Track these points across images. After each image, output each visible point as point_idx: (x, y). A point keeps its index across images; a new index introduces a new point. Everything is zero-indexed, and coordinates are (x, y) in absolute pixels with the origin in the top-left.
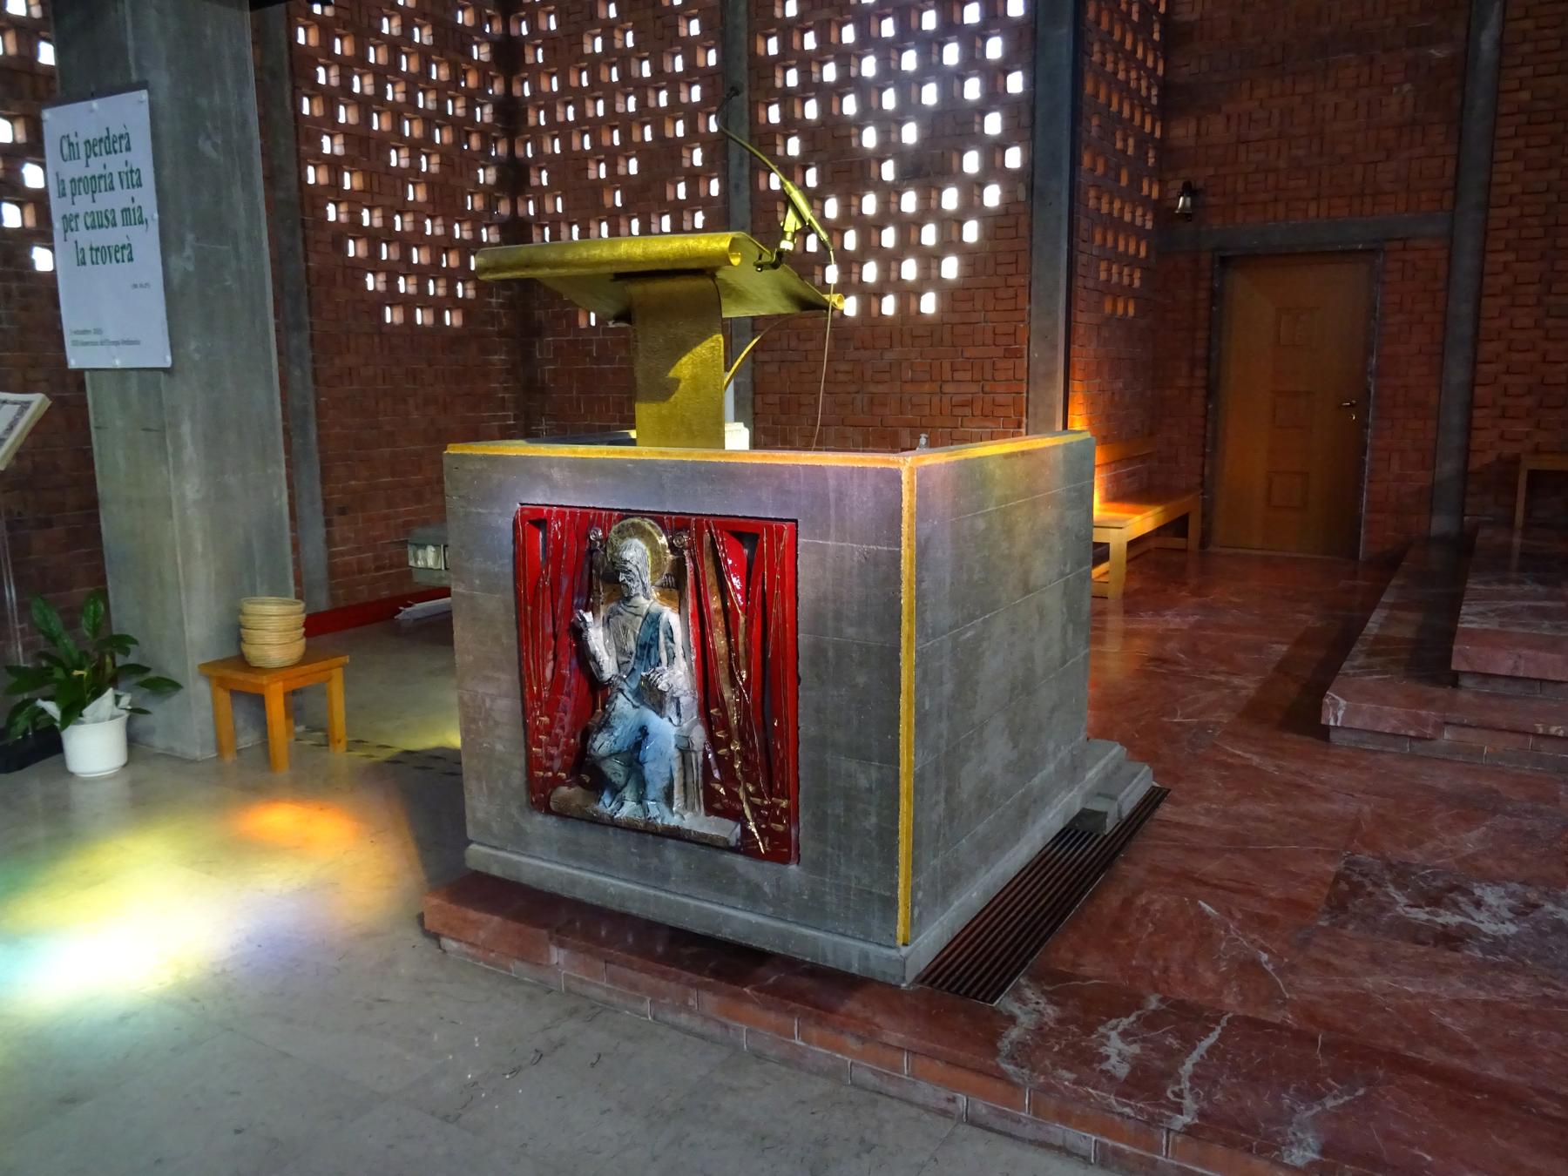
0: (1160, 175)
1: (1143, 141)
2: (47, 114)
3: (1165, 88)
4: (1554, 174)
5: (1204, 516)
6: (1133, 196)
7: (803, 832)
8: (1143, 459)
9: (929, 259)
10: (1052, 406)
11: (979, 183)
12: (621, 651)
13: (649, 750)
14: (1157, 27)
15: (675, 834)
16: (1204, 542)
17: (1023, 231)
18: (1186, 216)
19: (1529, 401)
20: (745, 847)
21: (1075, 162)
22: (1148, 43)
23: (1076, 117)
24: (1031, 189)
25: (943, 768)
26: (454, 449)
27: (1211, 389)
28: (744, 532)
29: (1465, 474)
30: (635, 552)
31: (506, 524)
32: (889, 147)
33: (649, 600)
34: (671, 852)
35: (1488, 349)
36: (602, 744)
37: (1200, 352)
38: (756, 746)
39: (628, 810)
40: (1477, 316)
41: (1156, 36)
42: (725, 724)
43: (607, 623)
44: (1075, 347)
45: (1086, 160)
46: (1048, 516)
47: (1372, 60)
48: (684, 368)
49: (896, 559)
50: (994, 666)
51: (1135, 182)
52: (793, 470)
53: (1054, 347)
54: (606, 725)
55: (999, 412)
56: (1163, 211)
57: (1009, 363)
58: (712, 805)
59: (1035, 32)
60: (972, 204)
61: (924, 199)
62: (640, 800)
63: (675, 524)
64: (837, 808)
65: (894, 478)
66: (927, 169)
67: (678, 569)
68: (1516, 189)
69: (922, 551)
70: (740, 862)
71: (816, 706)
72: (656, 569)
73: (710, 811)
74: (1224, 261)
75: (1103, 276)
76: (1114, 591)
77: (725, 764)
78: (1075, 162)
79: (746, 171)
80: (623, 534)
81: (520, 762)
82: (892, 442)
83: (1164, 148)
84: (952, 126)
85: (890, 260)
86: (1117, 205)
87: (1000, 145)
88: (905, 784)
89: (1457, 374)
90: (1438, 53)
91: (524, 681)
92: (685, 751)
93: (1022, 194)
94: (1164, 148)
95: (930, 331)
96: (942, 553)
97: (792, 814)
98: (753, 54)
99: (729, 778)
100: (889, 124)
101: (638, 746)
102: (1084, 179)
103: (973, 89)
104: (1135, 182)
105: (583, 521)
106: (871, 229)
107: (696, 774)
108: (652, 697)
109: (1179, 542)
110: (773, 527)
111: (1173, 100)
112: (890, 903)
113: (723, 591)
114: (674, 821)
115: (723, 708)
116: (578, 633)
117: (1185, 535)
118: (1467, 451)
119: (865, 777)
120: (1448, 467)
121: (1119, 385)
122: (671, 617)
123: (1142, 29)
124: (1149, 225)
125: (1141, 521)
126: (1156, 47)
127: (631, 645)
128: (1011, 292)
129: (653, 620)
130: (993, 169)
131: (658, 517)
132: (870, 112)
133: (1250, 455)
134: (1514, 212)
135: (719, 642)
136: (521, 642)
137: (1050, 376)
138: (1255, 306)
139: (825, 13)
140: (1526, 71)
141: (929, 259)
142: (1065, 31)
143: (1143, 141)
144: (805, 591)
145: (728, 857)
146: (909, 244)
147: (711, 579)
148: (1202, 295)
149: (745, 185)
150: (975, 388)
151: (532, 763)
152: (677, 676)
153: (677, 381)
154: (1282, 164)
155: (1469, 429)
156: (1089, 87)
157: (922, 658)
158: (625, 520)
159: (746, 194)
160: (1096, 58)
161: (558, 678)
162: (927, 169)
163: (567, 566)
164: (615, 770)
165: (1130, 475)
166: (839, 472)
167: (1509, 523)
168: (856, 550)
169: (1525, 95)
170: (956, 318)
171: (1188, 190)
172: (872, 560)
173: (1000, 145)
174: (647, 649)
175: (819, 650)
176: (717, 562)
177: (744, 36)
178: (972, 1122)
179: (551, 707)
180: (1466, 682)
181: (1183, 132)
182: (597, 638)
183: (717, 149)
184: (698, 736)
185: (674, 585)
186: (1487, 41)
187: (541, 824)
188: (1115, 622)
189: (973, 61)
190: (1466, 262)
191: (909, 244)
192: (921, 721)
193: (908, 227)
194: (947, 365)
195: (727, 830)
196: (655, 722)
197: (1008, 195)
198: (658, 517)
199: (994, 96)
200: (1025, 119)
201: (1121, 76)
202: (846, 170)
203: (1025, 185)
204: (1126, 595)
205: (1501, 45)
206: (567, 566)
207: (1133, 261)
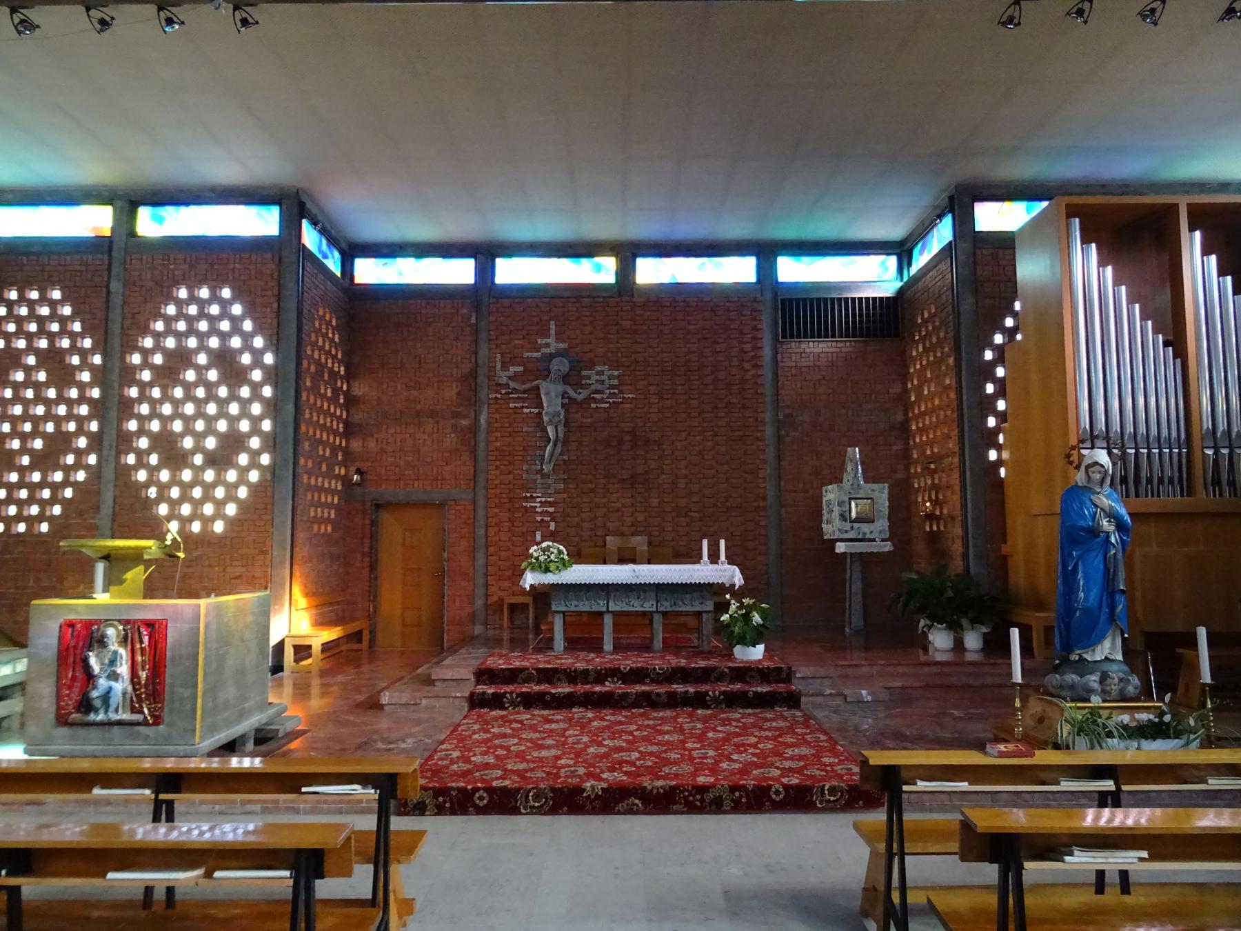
0: (344, 464)
1: (334, 450)
2: (472, 282)
3: (347, 423)
4: (511, 477)
5: (371, 632)
6: (330, 475)
7: (166, 715)
8: (330, 604)
9: (220, 504)
10: (283, 579)
11: (247, 469)
12: (102, 664)
13: (112, 694)
14: (342, 397)
15: (119, 723)
16: (372, 645)
17: (269, 494)
18: (358, 484)
19: (509, 573)
20: (145, 723)
21: (295, 463)
22: (337, 404)
23: (296, 442)
24: (274, 475)
25: (212, 691)
26: (34, 602)
27: (373, 567)
28: (149, 624)
29: (487, 606)
30: (111, 632)
31: (57, 627)
32: (198, 448)
33: (114, 646)
34: (116, 730)
35: (492, 549)
36: (94, 694)
37: (366, 550)
38: (152, 690)
39: (101, 717)
40: (487, 536)
41: (342, 401)
42: (139, 683)
43: (97, 656)
44: (296, 550)
45: (302, 461)
46: (250, 619)
47: (438, 422)
48: (129, 575)
49: (198, 628)
50: (231, 663)
51: (330, 468)
52: (167, 605)
53: (285, 549)
54: (95, 687)
55: (257, 581)
56: (347, 482)
57: (261, 557)
58: (133, 710)
59: (275, 405)
60: (242, 480)
61: (218, 475)
62: (106, 712)
63: (126, 622)
64: (177, 704)
65: (199, 606)
66: (219, 460)
67: (126, 637)
68: (497, 482)
69: (207, 626)
70: (142, 729)
71: (171, 674)
72: (118, 636)
73: (132, 712)
74: (378, 506)
75: (312, 514)
76: (315, 669)
77: (138, 696)
78: (295, 463)
79: (113, 453)
80: (106, 626)
81: (53, 709)
82: (198, 597)
83: (347, 452)
84: (233, 442)
85: (197, 504)
86: (320, 480)
87: (257, 453)
88: (200, 694)
89: (481, 561)
90: (464, 422)
91: (59, 679)
92: (124, 694)
93: (269, 477)
94: (347, 452)
95: (220, 541)
96: (213, 627)
97: (162, 708)
98: (121, 395)
99: (140, 701)
100: (199, 437)
101: (108, 692)
102: (300, 470)
103: (244, 426)
104: (330, 468)
105: (89, 624)
106: (186, 488)
107: (128, 700)
108: (114, 676)
109: (357, 646)
110: (159, 622)
111: (351, 429)
112: (194, 731)
113: (141, 642)
114: (119, 717)
115: (139, 678)
116: (85, 661)
117: (360, 642)
118: (487, 596)
119: (187, 693)
120: (479, 603)
121: (322, 566)
122: (122, 651)
123: (334, 400)
124: (339, 488)
125: (329, 635)
126: (341, 406)
127: (107, 661)
128: (262, 523)
129: (115, 653)
130: (254, 464)
131: (119, 621)
132: (188, 431)
133: (393, 600)
134: (498, 491)
135: (139, 658)
136: (59, 666)
137: (283, 563)
138: (393, 529)
139: (166, 381)
140: (498, 434)
141: (220, 504)
142: (290, 407)
143: (334, 450)
144: (169, 640)
145: (137, 728)
146: (207, 497)
147: (137, 638)
148: (367, 522)
149: (112, 459)
150: (243, 569)
151: (59, 708)
152: (123, 669)
153: (125, 580)
154: (402, 463)
155: (487, 586)
156: (303, 429)
157: (206, 657)
158: (108, 622)
159: (113, 465)
160: (307, 416)
161: (74, 678)
162: (219, 460)
163: (85, 636)
164: (97, 703)
165: (332, 611)
166: (182, 605)
167: (501, 627)
168: (186, 626)
169: (498, 444)
170: (234, 535)
171: (359, 472)
172: (191, 629)
173: (257, 453)
174: (113, 662)
175: (173, 658)
176: (140, 633)
177: (116, 385)
178: (221, 813)
179: (70, 687)
180: (437, 683)
181: (356, 445)
182: (93, 661)
183: (96, 442)
184: (130, 688)
185: (124, 641)
186: (483, 419)
187: (64, 731)
188: (315, 690)
189: (245, 413)
190: (481, 512)
191: (207, 497)
192: (205, 675)
193: (208, 488)
194: (228, 557)
195: (139, 717)
196: (113, 684)
197: (262, 475)
198: (119, 621)
199: (255, 430)
200: (271, 443)
201: (322, 421)
202: (174, 457)
203: (273, 469)
204: (321, 671)
205: (489, 424)
206: (85, 636)
207: (330, 506)
